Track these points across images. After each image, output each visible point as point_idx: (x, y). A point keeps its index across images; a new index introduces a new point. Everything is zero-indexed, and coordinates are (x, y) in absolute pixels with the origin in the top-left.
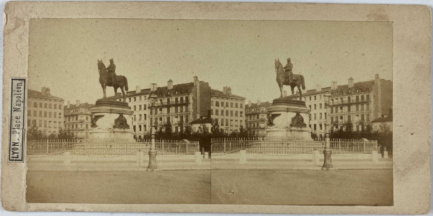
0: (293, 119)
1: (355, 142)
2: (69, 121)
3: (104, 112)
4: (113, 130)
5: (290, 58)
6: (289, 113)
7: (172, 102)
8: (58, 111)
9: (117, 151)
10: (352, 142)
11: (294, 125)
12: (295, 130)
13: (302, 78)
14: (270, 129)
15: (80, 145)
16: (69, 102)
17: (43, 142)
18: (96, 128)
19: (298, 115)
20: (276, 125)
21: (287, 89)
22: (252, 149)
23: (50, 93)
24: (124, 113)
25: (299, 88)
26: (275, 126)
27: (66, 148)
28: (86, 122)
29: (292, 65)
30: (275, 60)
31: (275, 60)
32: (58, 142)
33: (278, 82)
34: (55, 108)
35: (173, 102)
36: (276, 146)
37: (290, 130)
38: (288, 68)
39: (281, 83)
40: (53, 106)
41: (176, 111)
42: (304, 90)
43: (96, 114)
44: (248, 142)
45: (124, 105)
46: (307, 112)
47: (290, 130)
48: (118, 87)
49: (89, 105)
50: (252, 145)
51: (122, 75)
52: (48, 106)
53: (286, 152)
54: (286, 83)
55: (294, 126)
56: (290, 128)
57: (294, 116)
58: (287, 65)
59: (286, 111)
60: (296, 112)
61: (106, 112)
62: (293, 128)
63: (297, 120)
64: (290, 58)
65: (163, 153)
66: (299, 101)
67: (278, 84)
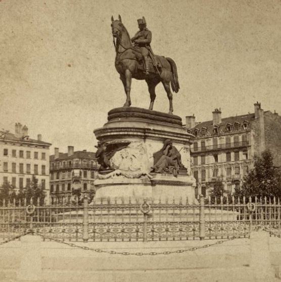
0: (157, 156)
1: (255, 205)
2: (58, 178)
6: (148, 142)
7: (221, 145)
8: (40, 163)
10: (244, 205)
11: (160, 169)
14: (103, 179)
15: (104, 215)
16: (73, 147)
19: (169, 146)
20: (118, 168)
21: (139, 86)
23: (98, 141)
25: (166, 86)
28: (84, 180)
30: (112, 19)
31: (112, 19)
34: (36, 157)
35: (211, 146)
37: (152, 181)
38: (143, 39)
39: (128, 72)
40: (32, 155)
41: (229, 158)
42: (176, 92)
46: (188, 140)
47: (150, 183)
49: (89, 153)
52: (25, 154)
53: (152, 237)
55: (159, 173)
56: (151, 177)
59: (141, 136)
60: (164, 140)
62: (159, 177)
63: (168, 157)
64: (143, 17)
66: (147, 110)
67: (118, 75)
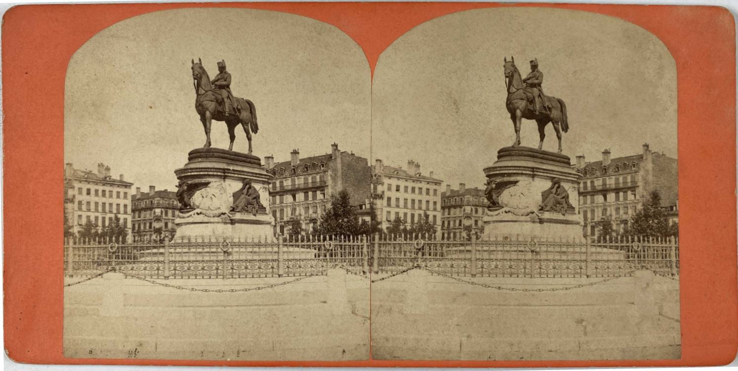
0: (545, 195)
3: (209, 175)
4: (538, 216)
5: (373, 63)
6: (228, 181)
9: (547, 267)
12: (551, 221)
13: (251, 106)
14: (183, 218)
17: (345, 241)
18: (500, 211)
20: (198, 207)
22: (449, 263)
24: (228, 176)
25: (246, 127)
26: (503, 210)
27: (638, 257)
29: (230, 75)
32: (87, 243)
33: (199, 112)
36: (515, 258)
37: (231, 220)
43: (499, 180)
44: (650, 247)
45: (236, 157)
48: (546, 123)
50: (141, 257)
51: (556, 97)
53: (232, 274)
54: (529, 114)
57: (547, 189)
58: (219, 77)
60: (243, 180)
61: (214, 176)
65: (281, 272)
66: (227, 151)
67: (199, 117)
